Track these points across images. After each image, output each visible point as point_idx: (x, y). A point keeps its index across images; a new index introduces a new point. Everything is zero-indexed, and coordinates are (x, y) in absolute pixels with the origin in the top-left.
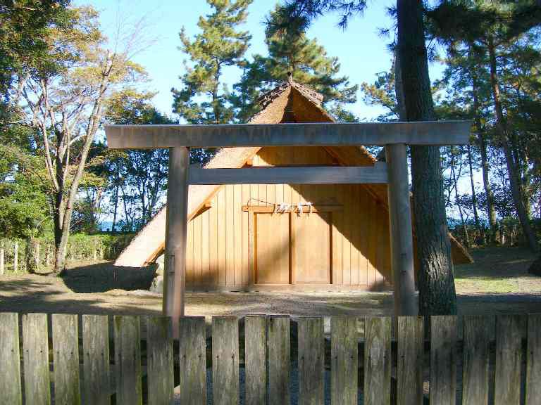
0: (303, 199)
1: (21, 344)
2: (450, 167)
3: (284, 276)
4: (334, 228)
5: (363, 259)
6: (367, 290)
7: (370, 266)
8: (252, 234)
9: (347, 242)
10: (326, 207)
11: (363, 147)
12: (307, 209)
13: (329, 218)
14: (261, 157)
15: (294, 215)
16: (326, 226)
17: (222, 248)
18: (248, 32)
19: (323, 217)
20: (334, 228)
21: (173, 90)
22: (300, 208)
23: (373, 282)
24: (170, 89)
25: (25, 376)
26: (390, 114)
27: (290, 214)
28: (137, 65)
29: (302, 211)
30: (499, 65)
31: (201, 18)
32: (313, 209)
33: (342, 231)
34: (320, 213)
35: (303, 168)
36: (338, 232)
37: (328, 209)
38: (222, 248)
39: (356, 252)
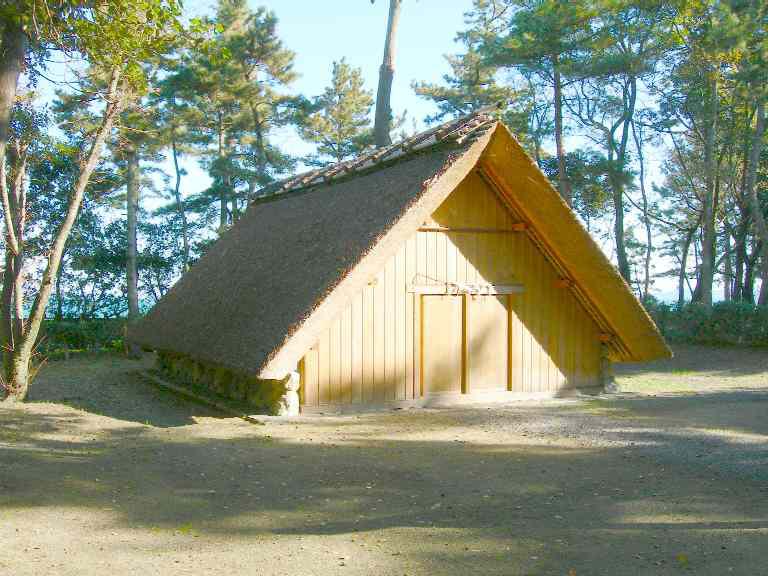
4: (514, 316)
5: (545, 356)
7: (552, 364)
8: (418, 326)
9: (527, 332)
11: (433, 508)
12: (484, 291)
15: (469, 298)
16: (504, 312)
17: (379, 352)
18: (261, 11)
20: (514, 316)
21: (445, 56)
24: (453, 43)
26: (586, 407)
27: (464, 296)
28: (299, 98)
32: (492, 290)
33: (523, 320)
35: (286, 537)
36: (518, 320)
38: (379, 352)
39: (537, 347)
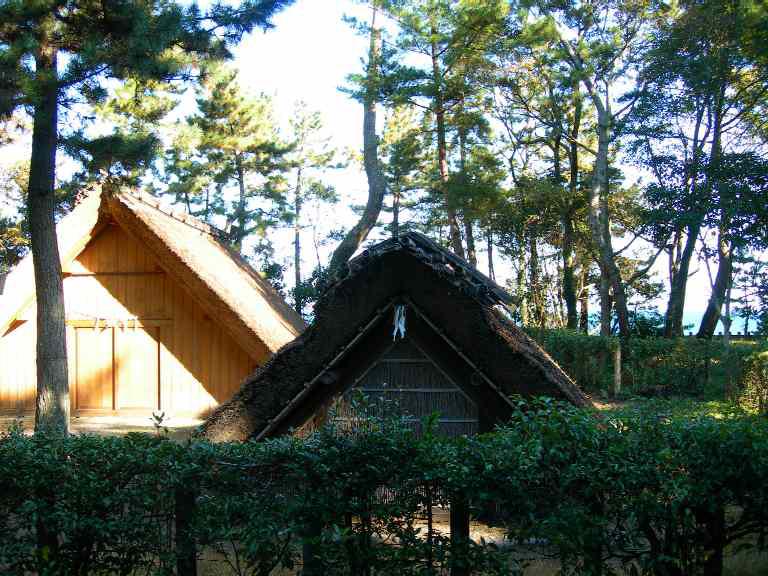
0: (127, 312)
1: (297, 260)
2: (401, 224)
3: (107, 402)
6: (200, 418)
10: (153, 322)
13: (157, 334)
14: (83, 264)
15: (118, 331)
16: (156, 343)
19: (150, 333)
22: (126, 325)
23: (207, 408)
25: (301, 271)
27: (113, 328)
29: (125, 326)
30: (156, 172)
31: (624, 178)
33: (172, 349)
34: (147, 328)
37: (156, 323)
